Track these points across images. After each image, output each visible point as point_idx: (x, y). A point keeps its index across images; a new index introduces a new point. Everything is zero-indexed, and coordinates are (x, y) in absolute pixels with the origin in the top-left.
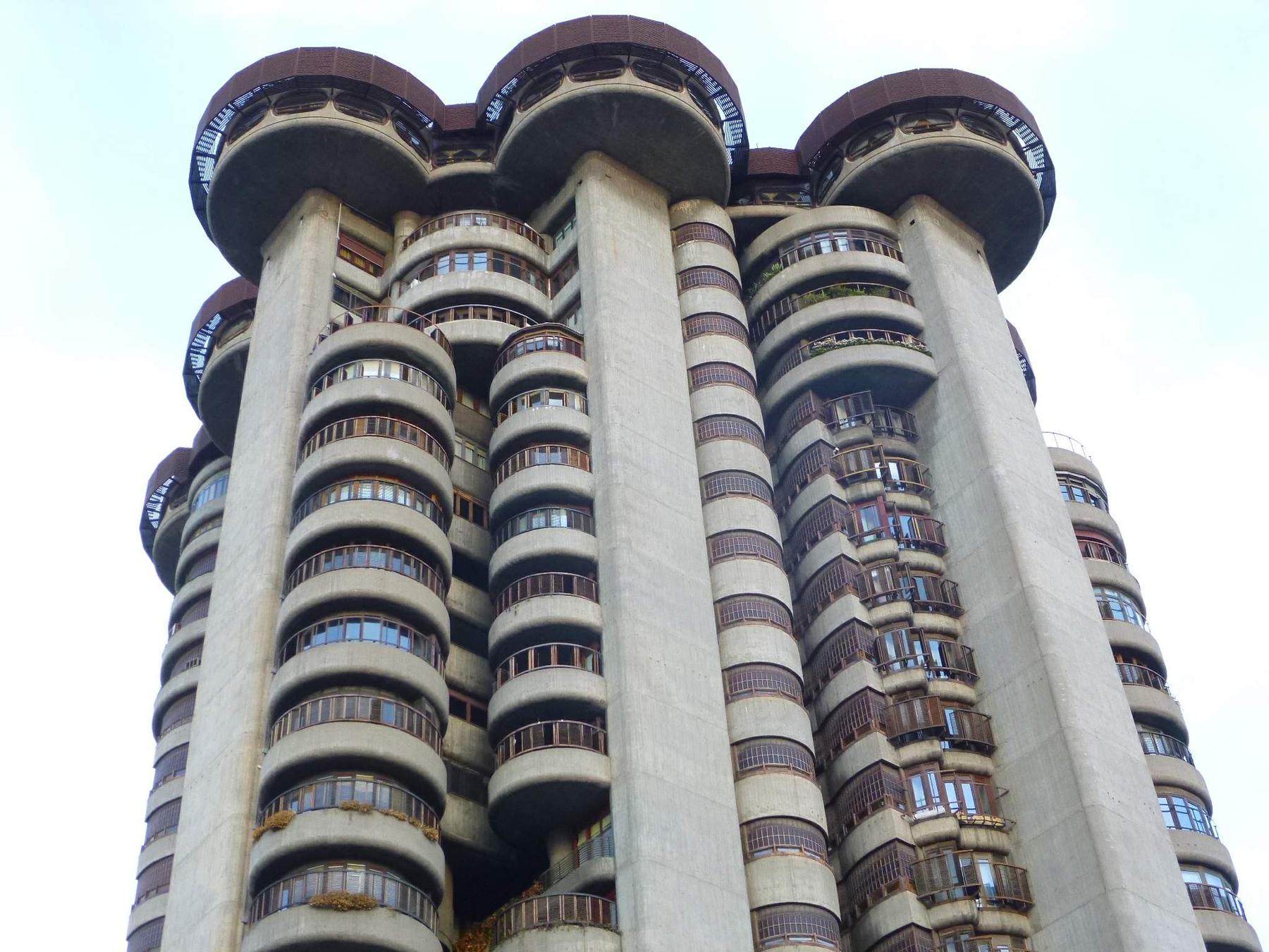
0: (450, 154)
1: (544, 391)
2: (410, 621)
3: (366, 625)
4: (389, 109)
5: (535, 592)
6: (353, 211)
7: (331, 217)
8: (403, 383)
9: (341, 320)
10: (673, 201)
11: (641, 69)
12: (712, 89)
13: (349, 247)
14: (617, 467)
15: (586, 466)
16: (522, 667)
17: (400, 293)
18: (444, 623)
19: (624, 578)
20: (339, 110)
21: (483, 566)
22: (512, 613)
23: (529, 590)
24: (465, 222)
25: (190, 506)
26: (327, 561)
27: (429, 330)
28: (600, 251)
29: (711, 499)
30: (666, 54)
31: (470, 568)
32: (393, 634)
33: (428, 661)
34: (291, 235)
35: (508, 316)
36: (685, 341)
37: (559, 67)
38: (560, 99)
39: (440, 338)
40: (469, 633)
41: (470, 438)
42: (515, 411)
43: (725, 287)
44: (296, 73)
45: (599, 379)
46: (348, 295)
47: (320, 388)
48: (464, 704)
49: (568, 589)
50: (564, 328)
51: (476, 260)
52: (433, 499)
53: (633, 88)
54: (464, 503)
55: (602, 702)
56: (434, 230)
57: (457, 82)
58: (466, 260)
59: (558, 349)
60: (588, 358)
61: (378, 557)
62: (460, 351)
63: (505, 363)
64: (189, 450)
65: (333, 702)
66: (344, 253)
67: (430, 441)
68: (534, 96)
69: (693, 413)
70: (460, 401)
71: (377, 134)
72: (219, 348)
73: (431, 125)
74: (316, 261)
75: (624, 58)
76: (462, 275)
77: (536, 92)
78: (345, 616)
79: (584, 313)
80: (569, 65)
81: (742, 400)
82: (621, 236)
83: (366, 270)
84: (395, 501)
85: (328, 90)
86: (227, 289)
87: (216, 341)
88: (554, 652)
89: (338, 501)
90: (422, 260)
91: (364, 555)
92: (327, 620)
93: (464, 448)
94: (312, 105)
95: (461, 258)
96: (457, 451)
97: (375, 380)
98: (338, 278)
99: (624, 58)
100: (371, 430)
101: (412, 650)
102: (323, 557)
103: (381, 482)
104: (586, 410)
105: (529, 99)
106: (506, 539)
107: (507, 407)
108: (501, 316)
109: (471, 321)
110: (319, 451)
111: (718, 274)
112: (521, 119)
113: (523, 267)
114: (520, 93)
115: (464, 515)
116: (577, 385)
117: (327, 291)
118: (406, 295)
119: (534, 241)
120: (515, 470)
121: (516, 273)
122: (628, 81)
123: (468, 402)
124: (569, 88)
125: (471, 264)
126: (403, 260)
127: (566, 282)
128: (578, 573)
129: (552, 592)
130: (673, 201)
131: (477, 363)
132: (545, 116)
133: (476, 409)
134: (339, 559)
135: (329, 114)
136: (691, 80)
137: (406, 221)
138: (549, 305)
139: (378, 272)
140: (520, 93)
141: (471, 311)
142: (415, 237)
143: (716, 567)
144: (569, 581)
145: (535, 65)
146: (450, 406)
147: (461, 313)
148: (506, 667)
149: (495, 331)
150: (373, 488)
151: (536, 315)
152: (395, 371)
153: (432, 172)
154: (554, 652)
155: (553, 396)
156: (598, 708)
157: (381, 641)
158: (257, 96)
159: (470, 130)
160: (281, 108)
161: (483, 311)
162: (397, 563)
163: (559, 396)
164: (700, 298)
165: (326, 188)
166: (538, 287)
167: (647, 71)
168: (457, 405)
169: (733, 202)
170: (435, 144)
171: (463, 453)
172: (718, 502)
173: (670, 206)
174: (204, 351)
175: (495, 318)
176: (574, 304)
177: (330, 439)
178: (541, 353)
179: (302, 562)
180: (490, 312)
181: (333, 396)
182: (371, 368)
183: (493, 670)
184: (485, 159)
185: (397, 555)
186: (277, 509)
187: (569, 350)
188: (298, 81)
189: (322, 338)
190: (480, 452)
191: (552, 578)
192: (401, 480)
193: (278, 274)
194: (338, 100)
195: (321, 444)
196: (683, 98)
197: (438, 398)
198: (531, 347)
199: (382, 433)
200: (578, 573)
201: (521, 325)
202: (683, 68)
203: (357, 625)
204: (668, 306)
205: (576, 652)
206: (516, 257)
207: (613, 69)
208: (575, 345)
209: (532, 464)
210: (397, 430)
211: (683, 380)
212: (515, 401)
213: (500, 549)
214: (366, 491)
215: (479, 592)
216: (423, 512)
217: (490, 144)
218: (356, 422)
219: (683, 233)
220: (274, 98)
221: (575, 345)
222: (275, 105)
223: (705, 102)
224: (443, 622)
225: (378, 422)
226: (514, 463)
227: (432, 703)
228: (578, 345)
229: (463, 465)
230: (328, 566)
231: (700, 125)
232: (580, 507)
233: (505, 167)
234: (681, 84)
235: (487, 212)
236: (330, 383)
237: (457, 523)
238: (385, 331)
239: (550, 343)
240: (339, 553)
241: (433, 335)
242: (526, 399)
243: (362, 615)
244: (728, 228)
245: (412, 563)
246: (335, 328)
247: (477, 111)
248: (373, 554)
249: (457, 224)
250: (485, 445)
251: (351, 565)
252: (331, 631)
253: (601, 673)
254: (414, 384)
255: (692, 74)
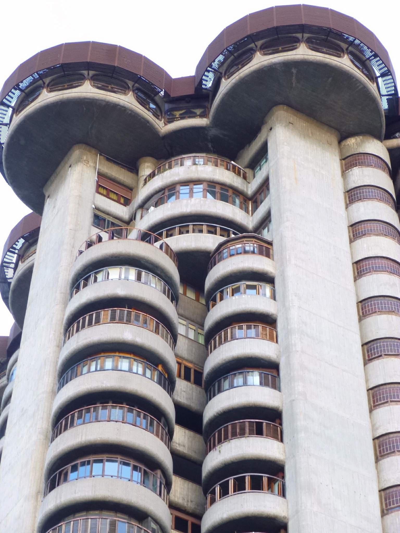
0: (177, 114)
1: (243, 284)
2: (144, 462)
3: (107, 464)
4: (130, 84)
5: (234, 435)
6: (108, 159)
7: (91, 164)
8: (137, 283)
9: (94, 238)
10: (342, 138)
11: (312, 43)
12: (368, 54)
13: (105, 185)
14: (295, 339)
15: (273, 338)
16: (225, 492)
17: (142, 217)
18: (167, 460)
19: (301, 423)
20: (94, 86)
21: (199, 416)
22: (217, 452)
23: (230, 435)
24: (188, 163)
25: (8, 379)
26: (80, 417)
27: (158, 244)
28: (284, 179)
29: (371, 360)
30: (334, 33)
31: (188, 417)
32: (127, 470)
33: (154, 490)
34: (64, 178)
35: (218, 229)
36: (351, 241)
37: (252, 45)
38: (253, 69)
39: (167, 250)
40: (187, 467)
41: (193, 321)
42: (221, 299)
43: (386, 202)
44: (61, 62)
45: (283, 273)
46: (104, 220)
47: (78, 288)
48: (186, 521)
49: (259, 432)
50: (259, 238)
51: (195, 190)
52: (160, 368)
53: (306, 57)
54: (187, 370)
55: (285, 518)
56: (165, 170)
57: (180, 60)
58: (188, 191)
59: (253, 252)
60: (275, 257)
61: (117, 412)
62: (185, 259)
63: (215, 264)
64: (7, 338)
65: (81, 523)
66: (101, 190)
67: (157, 324)
68: (235, 67)
69: (357, 295)
70: (185, 294)
71: (122, 103)
72: (23, 262)
73: (162, 93)
74: (80, 196)
75: (299, 35)
76: (185, 202)
77: (237, 65)
78: (91, 458)
79: (273, 225)
80: (259, 43)
81: (394, 284)
82: (301, 165)
83: (118, 201)
84: (130, 370)
85: (85, 72)
86: (26, 219)
87: (21, 257)
88: (247, 480)
89: (89, 371)
90: (157, 192)
91: (107, 411)
92: (79, 461)
93: (188, 328)
94: (75, 84)
95: (184, 190)
96: (181, 330)
97: (118, 282)
98: (97, 209)
99: (299, 35)
100: (113, 319)
101: (144, 483)
102: (76, 415)
103: (120, 357)
104: (274, 297)
105: (232, 70)
106: (214, 395)
107: (215, 297)
108: (213, 230)
109: (191, 235)
110: (76, 335)
111: (376, 191)
112: (226, 85)
113: (230, 193)
114: (226, 65)
115: (187, 378)
116: (268, 279)
117: (88, 218)
118: (145, 218)
119: (239, 174)
120: (220, 343)
121: (224, 198)
122: (303, 52)
123: (191, 295)
124: (259, 61)
125: (191, 193)
126: (144, 192)
127: (261, 203)
128: (266, 420)
129: (246, 436)
130: (342, 138)
131: (194, 266)
132: (243, 82)
133: (197, 300)
134: (88, 415)
135: (87, 90)
136: (350, 48)
137: (147, 164)
138: (249, 221)
139: (127, 202)
140: (226, 65)
141: (191, 228)
142: (152, 175)
143: (375, 412)
144: (259, 426)
145: (236, 45)
146: (174, 298)
147: (183, 230)
148: (213, 492)
149: (207, 241)
150: (113, 361)
151: (239, 228)
152: (132, 273)
153: (164, 127)
154: (247, 480)
155: (249, 287)
156: (282, 522)
157: (118, 477)
158: (35, 81)
159: (194, 96)
160: (52, 87)
161: (199, 227)
162: (130, 417)
163: (254, 287)
164: (362, 210)
165: (87, 144)
166: (241, 208)
167: (317, 44)
168: (181, 297)
169: (389, 136)
170: (167, 106)
171: (187, 332)
172: (376, 363)
173: (340, 142)
174: (12, 266)
175: (209, 232)
176: (266, 220)
177: (83, 327)
178: (239, 256)
179: (64, 417)
180: (205, 228)
181: (88, 294)
182: (114, 273)
183: (205, 493)
184: (202, 116)
185: (130, 411)
186: (49, 377)
187: (261, 253)
188: (64, 67)
189: (81, 252)
190: (200, 331)
191: (247, 424)
192: (135, 354)
193: (54, 207)
194: (94, 79)
195: (78, 330)
196: (345, 63)
197: (164, 293)
198: (232, 252)
199: (121, 321)
200: (266, 420)
201: (229, 236)
202: (345, 41)
203: (101, 465)
204: (339, 217)
205: (265, 480)
206: (225, 187)
207: (291, 44)
208: (266, 249)
209: (233, 338)
210: (133, 317)
211: (349, 272)
212: (222, 292)
213: (210, 403)
214: (109, 363)
215: (198, 436)
216: (152, 379)
217: (206, 104)
218: (102, 313)
219: (350, 161)
220: (47, 80)
221: (266, 249)
222: (48, 85)
223: (363, 64)
224: (167, 460)
225: (118, 312)
226: (220, 338)
227: (156, 522)
228: (268, 249)
229: (187, 341)
230: (81, 421)
231: (358, 81)
232: (269, 370)
233: (216, 122)
234: (343, 51)
235: (204, 155)
236: (85, 285)
237: (182, 386)
238: (130, 245)
239: (247, 248)
240: (88, 411)
241: (161, 247)
242: (230, 290)
243: (104, 457)
244: (386, 157)
245: (142, 415)
246: (90, 245)
247: (197, 81)
248: (113, 411)
249: (182, 165)
250: (202, 325)
251: (97, 420)
252: (81, 469)
253: (284, 495)
254: (146, 283)
255: (351, 44)
